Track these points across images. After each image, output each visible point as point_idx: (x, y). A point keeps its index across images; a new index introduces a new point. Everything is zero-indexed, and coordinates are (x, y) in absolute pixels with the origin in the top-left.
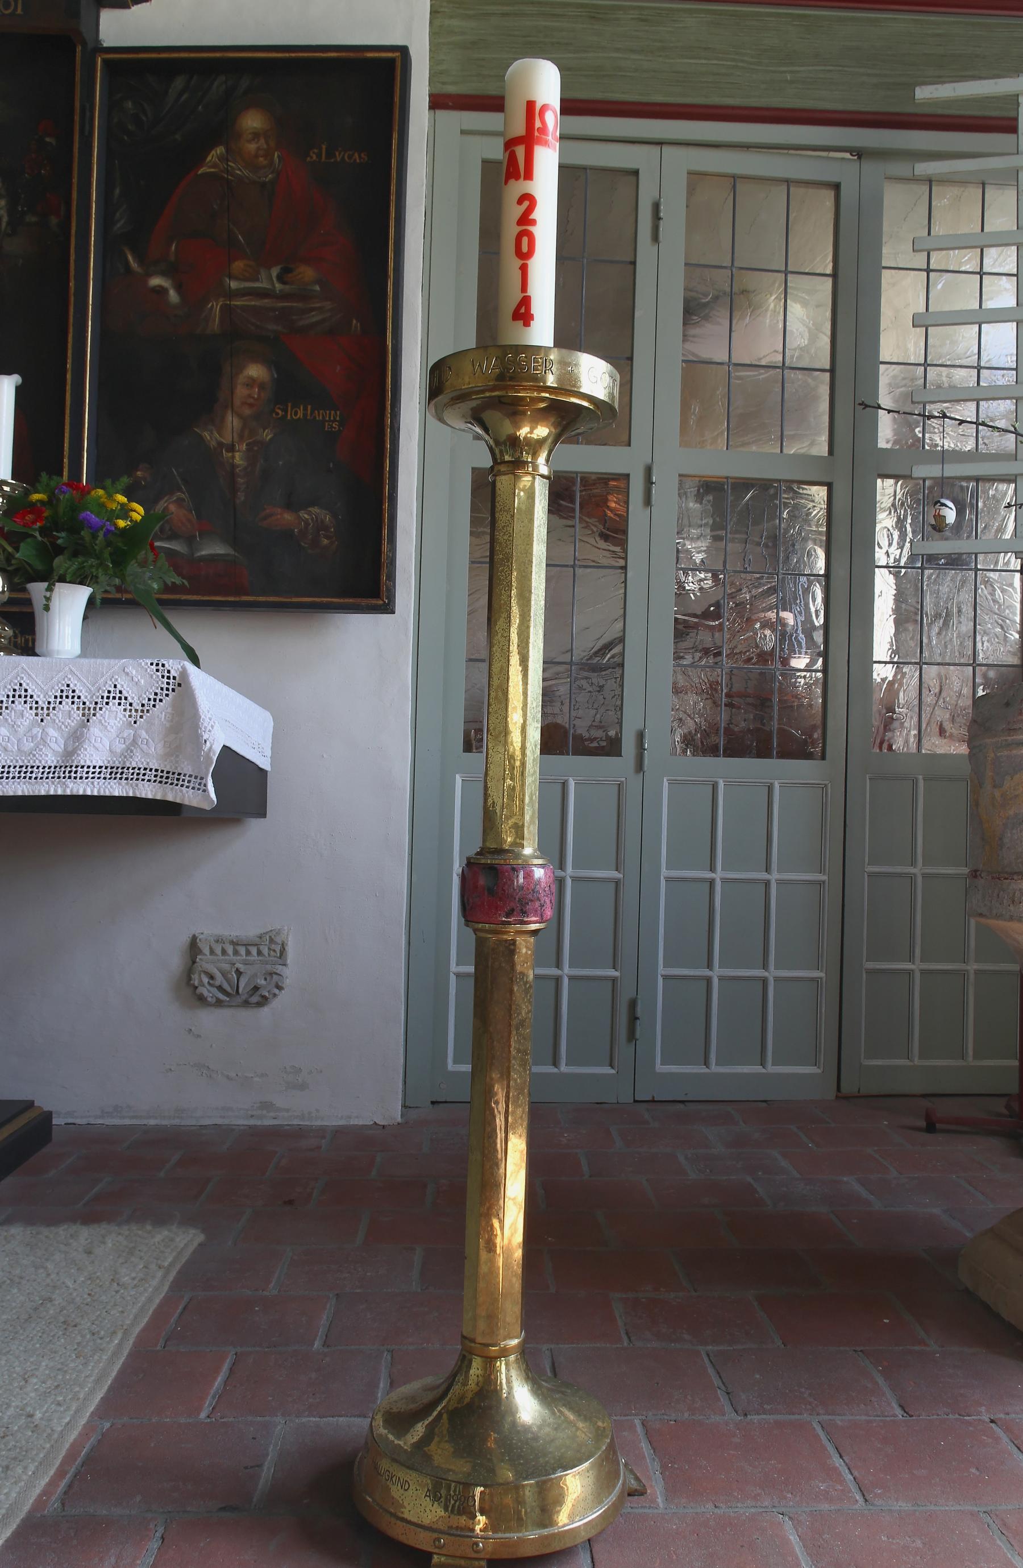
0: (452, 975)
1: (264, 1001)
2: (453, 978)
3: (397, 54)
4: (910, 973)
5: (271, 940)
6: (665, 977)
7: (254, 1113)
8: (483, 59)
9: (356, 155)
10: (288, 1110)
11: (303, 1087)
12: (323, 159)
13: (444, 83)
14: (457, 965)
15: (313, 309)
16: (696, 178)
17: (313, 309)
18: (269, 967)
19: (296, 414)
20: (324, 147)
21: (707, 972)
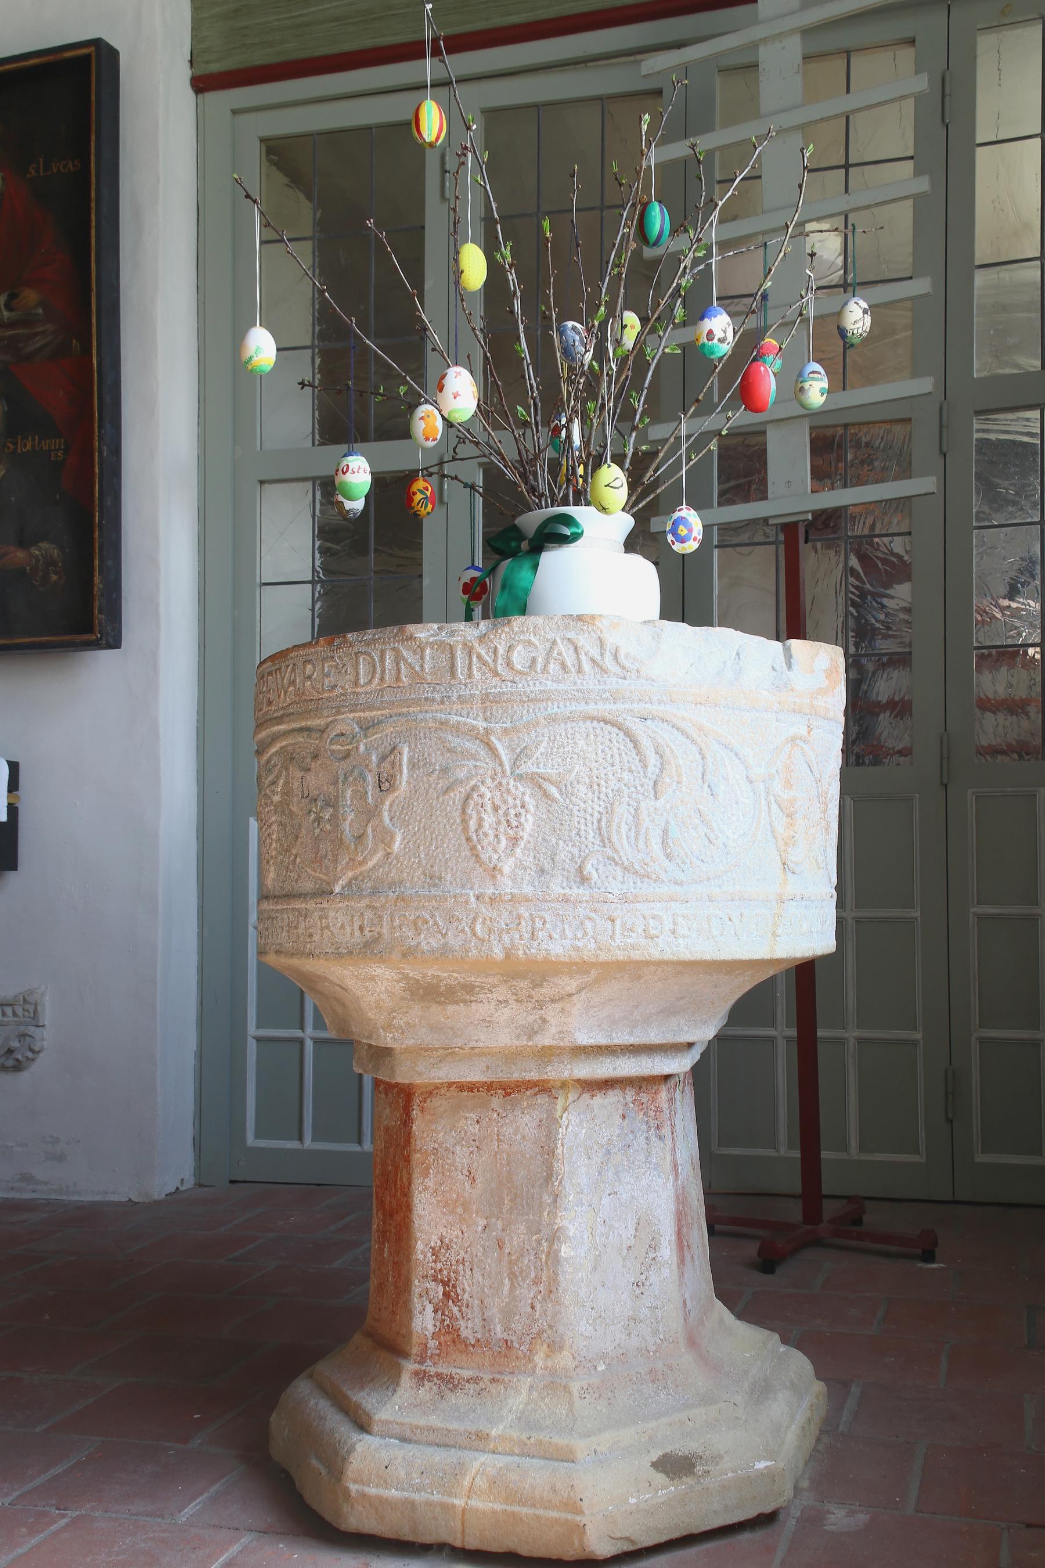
2: (252, 1046)
3: (92, 49)
4: (771, 1040)
6: (259, 1039)
8: (246, 27)
9: (70, 163)
10: (46, 1183)
11: (61, 1158)
12: (41, 174)
13: (208, 62)
14: (258, 1027)
15: (36, 334)
17: (36, 334)
18: (22, 1029)
19: (25, 446)
20: (41, 160)
21: (298, 1033)
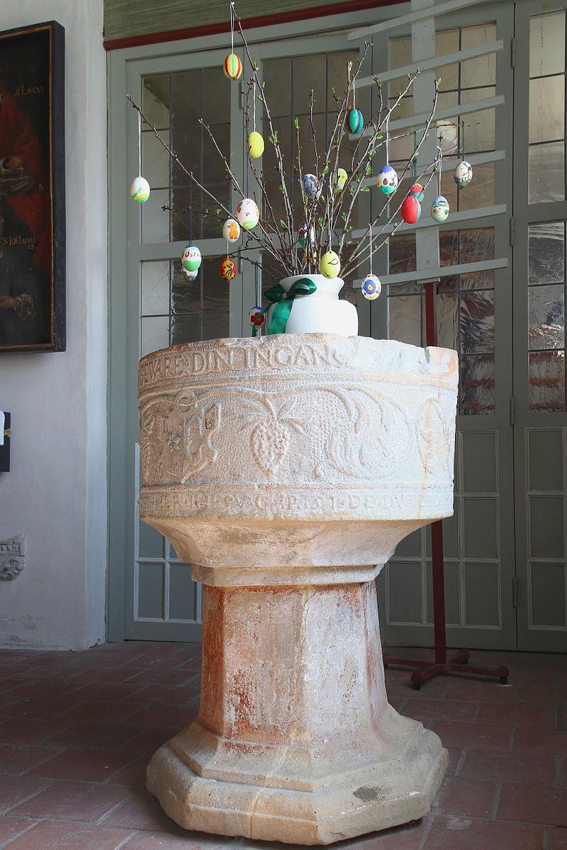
0: (135, 563)
1: (10, 578)
2: (137, 566)
4: (419, 563)
5: (14, 542)
7: (8, 642)
10: (25, 641)
11: (33, 627)
13: (112, 34)
15: (20, 181)
16: (267, 63)
17: (20, 181)
18: (12, 557)
21: (162, 560)
